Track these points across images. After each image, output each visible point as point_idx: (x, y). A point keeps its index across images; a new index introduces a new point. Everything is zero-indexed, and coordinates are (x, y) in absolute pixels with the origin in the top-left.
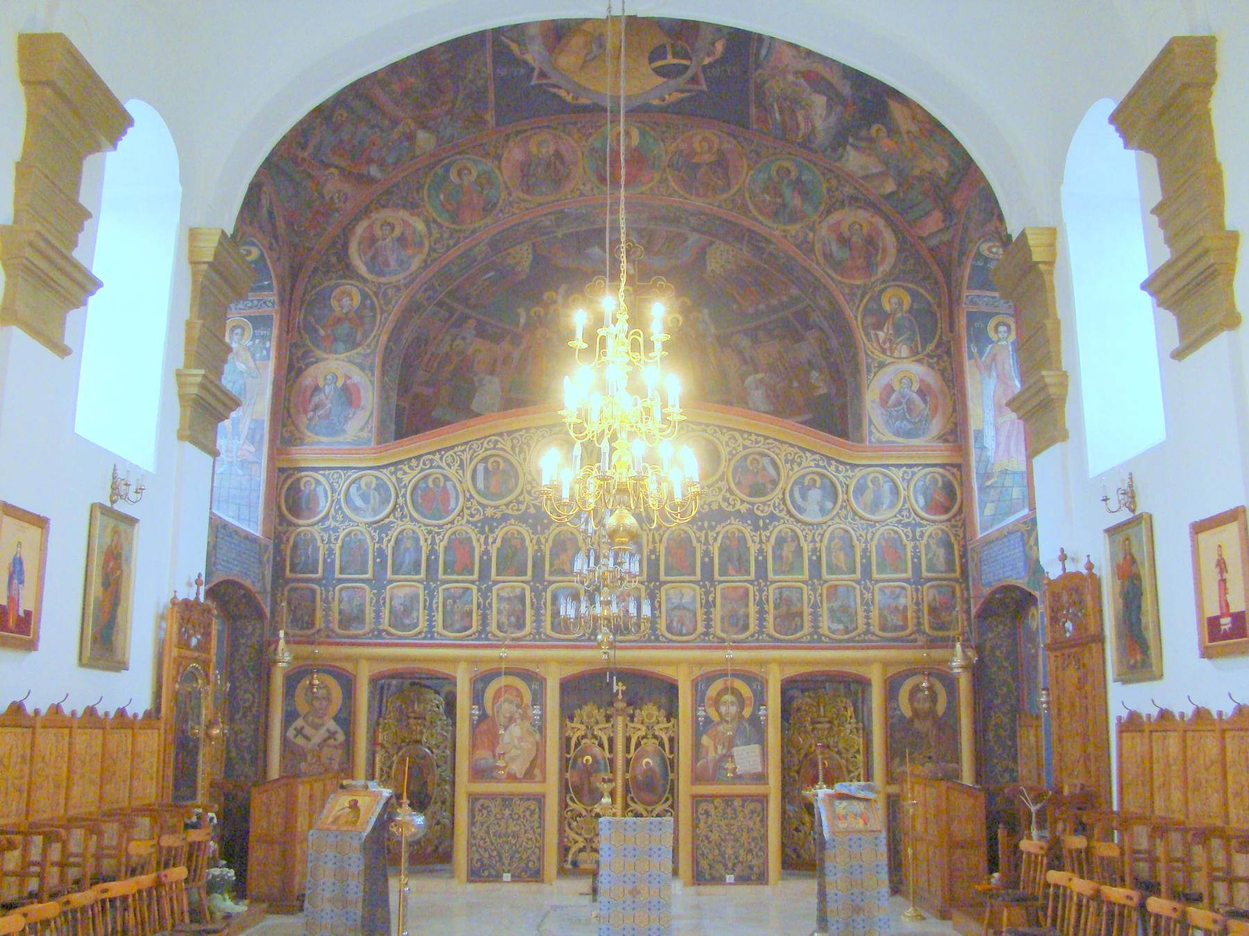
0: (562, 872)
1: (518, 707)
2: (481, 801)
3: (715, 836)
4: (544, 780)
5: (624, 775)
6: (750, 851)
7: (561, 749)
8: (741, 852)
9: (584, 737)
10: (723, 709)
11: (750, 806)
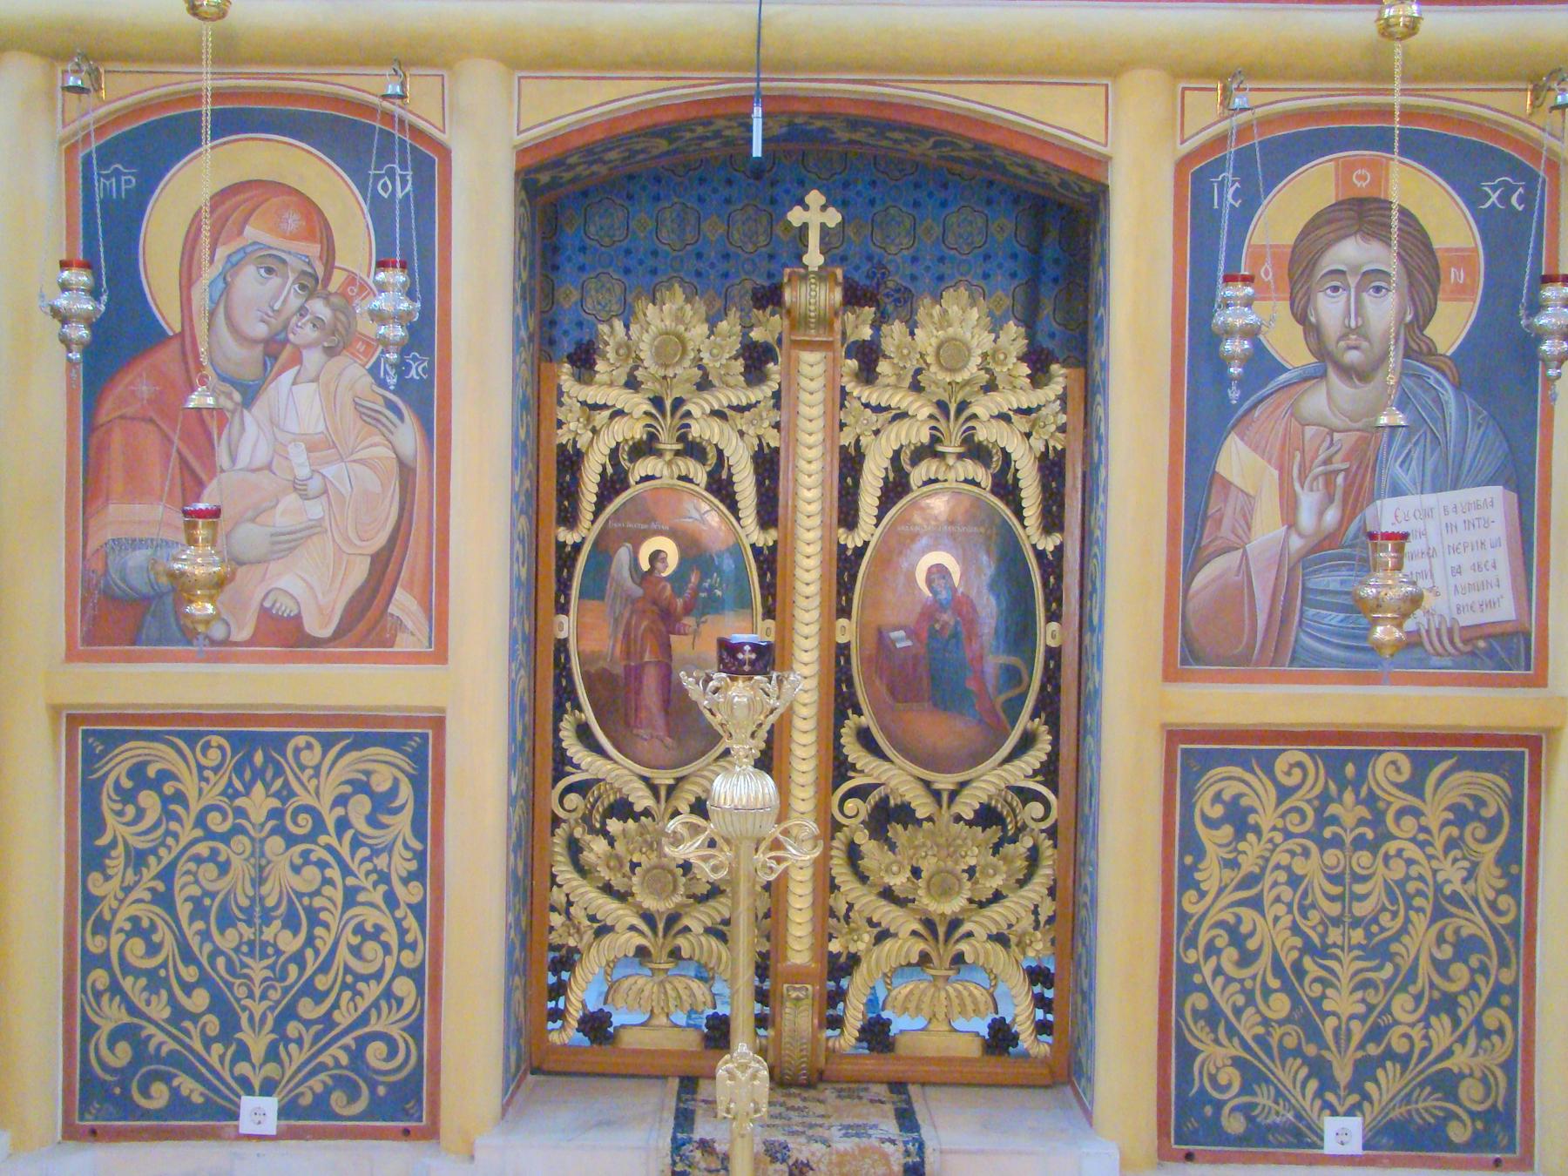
0: (533, 1066)
1: (312, 285)
2: (134, 751)
3: (1272, 932)
4: (439, 654)
5: (827, 632)
6: (1447, 1004)
7: (528, 502)
8: (1402, 1006)
9: (646, 448)
10: (1330, 309)
11: (1451, 787)
